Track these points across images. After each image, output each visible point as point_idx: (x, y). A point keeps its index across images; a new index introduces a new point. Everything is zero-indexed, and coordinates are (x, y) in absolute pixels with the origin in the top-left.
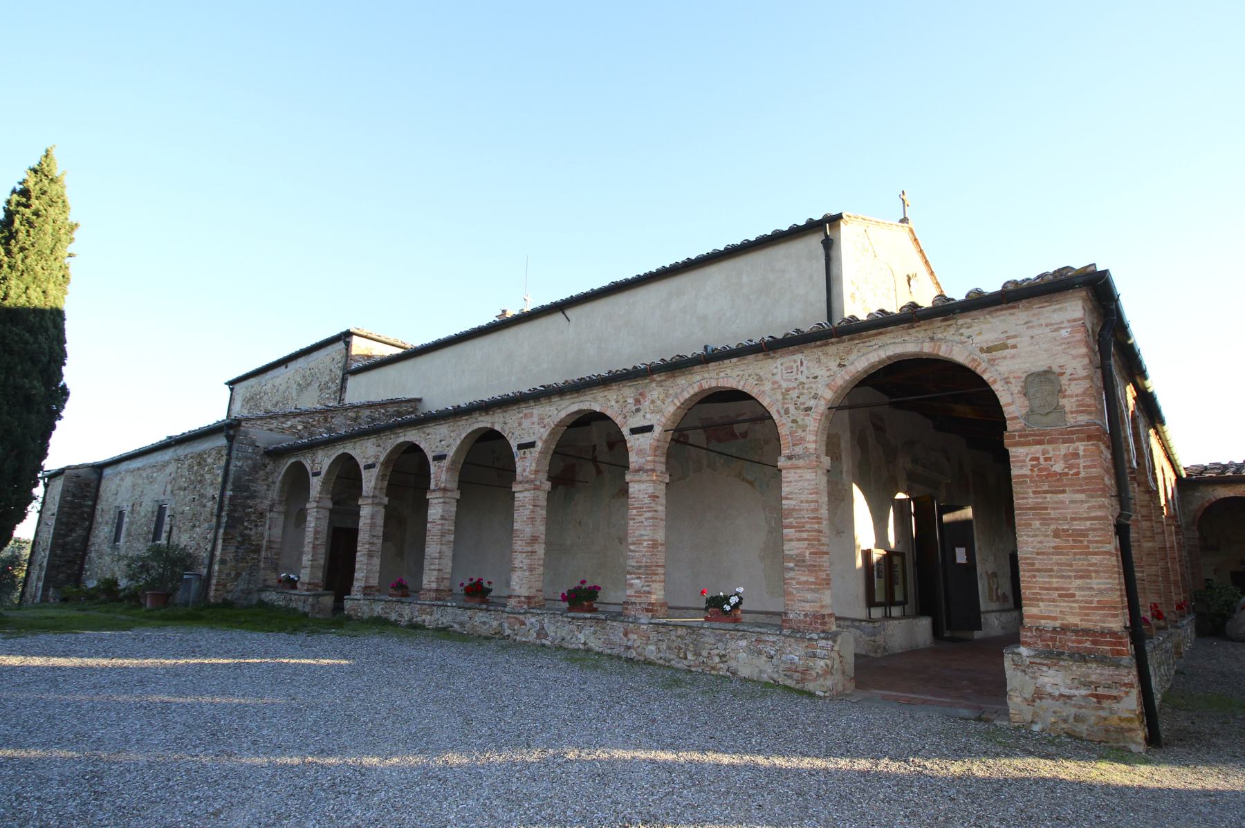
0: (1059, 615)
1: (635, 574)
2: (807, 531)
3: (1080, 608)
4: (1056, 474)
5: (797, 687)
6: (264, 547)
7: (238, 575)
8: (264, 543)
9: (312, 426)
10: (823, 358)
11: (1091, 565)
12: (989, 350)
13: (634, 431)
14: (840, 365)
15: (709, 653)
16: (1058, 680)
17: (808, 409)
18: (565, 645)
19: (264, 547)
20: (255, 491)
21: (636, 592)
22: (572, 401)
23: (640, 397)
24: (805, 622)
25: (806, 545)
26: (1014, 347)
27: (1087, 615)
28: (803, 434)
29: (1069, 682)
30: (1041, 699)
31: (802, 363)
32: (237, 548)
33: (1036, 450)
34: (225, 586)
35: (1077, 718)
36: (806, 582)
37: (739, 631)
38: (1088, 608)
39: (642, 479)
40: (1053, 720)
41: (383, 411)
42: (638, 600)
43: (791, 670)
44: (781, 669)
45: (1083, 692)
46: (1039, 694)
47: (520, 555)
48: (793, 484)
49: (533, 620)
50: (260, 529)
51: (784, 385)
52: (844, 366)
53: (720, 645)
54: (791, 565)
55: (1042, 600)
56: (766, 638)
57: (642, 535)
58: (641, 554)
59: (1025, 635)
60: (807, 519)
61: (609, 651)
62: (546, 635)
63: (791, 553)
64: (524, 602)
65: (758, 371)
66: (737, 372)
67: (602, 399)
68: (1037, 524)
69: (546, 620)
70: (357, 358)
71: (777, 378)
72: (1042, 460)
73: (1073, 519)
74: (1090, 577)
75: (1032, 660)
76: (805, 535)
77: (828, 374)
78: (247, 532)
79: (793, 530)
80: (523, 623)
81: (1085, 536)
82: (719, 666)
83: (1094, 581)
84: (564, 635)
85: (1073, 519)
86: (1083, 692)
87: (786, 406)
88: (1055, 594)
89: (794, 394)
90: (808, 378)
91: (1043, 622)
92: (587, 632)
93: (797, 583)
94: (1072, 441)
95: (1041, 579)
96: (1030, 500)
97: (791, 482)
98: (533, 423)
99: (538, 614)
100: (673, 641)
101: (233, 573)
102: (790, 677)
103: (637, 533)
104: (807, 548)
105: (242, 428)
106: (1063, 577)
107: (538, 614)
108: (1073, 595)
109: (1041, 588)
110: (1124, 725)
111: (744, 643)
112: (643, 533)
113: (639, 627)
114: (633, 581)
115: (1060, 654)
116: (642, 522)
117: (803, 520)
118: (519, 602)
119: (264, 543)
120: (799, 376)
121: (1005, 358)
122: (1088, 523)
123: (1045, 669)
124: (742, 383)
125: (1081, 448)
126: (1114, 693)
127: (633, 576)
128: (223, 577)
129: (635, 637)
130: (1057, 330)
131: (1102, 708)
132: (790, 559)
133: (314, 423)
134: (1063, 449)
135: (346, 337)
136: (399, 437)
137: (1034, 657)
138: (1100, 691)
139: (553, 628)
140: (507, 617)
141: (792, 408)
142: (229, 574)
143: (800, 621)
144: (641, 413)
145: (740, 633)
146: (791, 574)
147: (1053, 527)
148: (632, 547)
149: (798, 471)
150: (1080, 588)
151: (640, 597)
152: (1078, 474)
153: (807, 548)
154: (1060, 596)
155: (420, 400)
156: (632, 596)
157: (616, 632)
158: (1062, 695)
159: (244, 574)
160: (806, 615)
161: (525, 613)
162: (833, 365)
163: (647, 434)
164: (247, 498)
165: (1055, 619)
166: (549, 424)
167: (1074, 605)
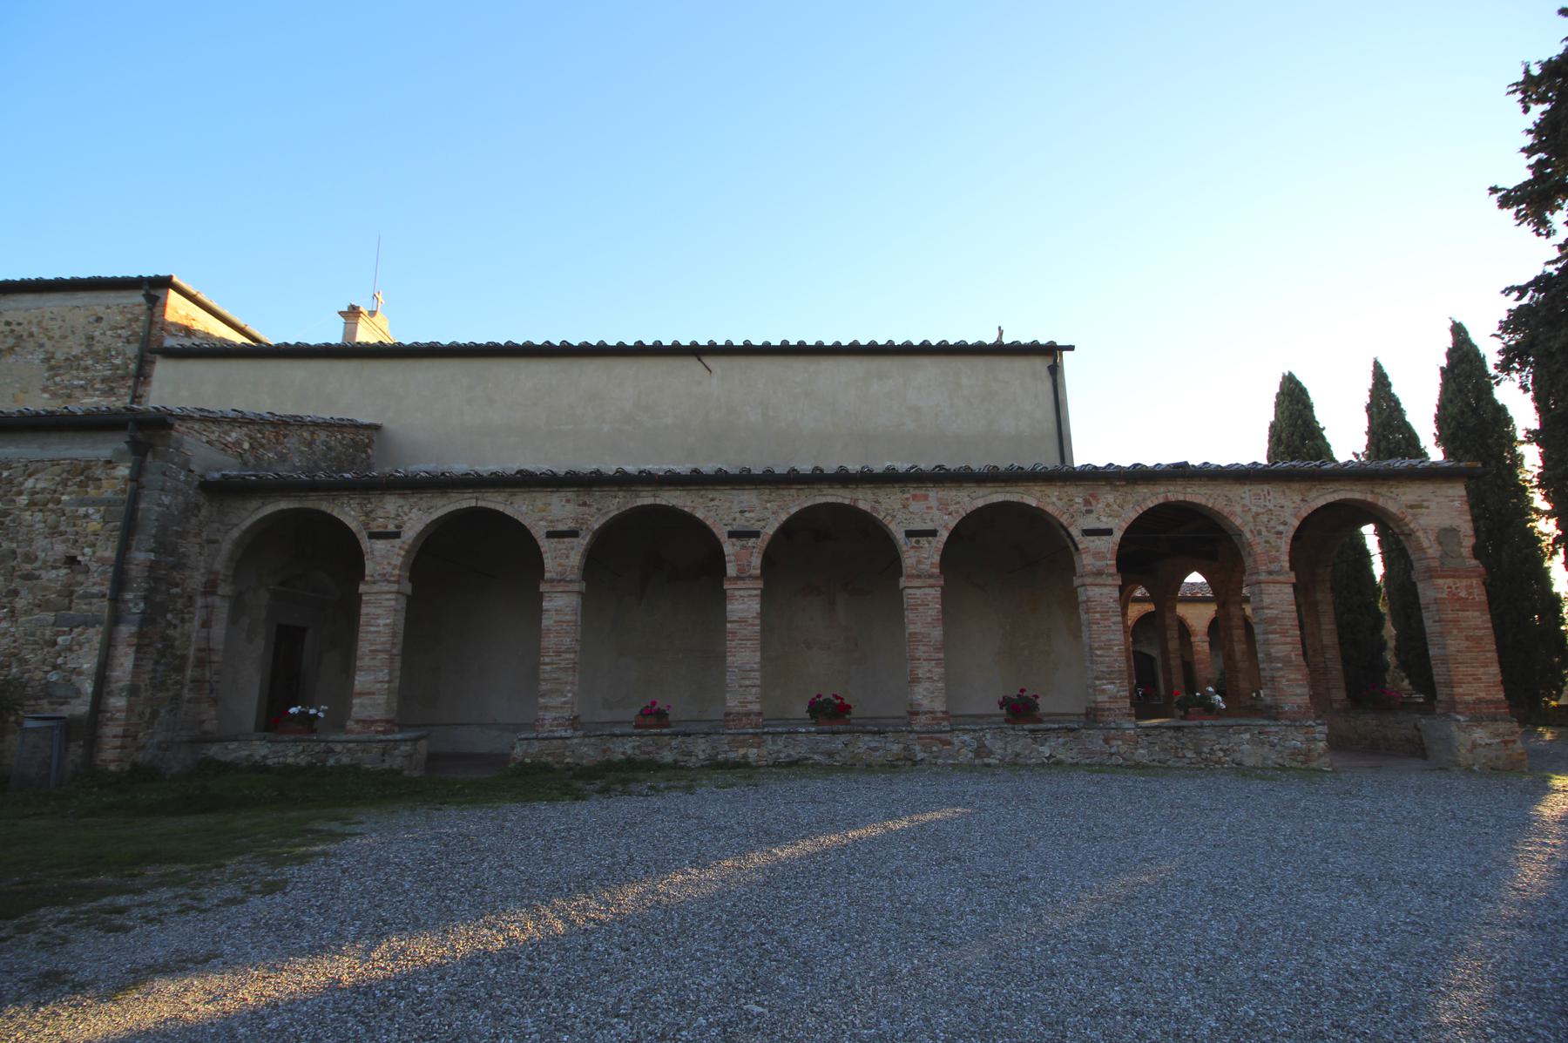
0: (1473, 692)
1: (1106, 679)
2: (1291, 636)
3: (1485, 686)
4: (1462, 598)
5: (1303, 767)
6: (191, 660)
7: (155, 714)
8: (191, 652)
9: (262, 446)
10: (1287, 491)
11: (1487, 658)
12: (1411, 507)
13: (1088, 533)
14: (1303, 500)
15: (1212, 749)
16: (1482, 735)
17: (1280, 533)
18: (1021, 761)
19: (191, 660)
20: (184, 555)
21: (1110, 697)
22: (994, 489)
23: (1091, 499)
24: (1299, 713)
25: (1291, 649)
26: (1427, 508)
27: (1489, 691)
28: (1277, 554)
29: (1488, 734)
30: (1475, 748)
31: (1269, 493)
32: (157, 662)
33: (1450, 581)
34: (135, 738)
35: (1497, 758)
36: (1296, 679)
37: (1241, 725)
38: (1489, 686)
39: (1107, 583)
40: (1484, 761)
41: (339, 437)
42: (1113, 706)
43: (1295, 753)
44: (1285, 754)
45: (1498, 740)
46: (1475, 746)
47: (925, 663)
48: (1273, 596)
49: (966, 737)
50: (187, 626)
51: (1254, 509)
52: (1306, 501)
53: (1222, 740)
54: (1280, 665)
55: (1464, 683)
56: (1268, 729)
57: (1110, 640)
58: (1112, 659)
59: (1460, 707)
60: (1289, 627)
61: (1088, 761)
62: (990, 754)
63: (1279, 655)
64: (943, 719)
65: (1227, 493)
66: (1204, 490)
67: (1039, 494)
68: (1455, 632)
69: (988, 736)
70: (173, 329)
71: (1247, 502)
72: (1454, 589)
73: (1475, 629)
74: (1487, 666)
75: (1470, 723)
76: (1289, 640)
77: (1293, 505)
78: (170, 632)
79: (1277, 636)
80: (950, 743)
81: (1482, 639)
82: (1223, 759)
83: (1491, 669)
84: (1018, 750)
85: (1475, 629)
86: (1498, 740)
87: (1258, 528)
88: (1470, 678)
89: (1265, 518)
90: (1275, 506)
91: (1466, 697)
92: (1053, 744)
93: (1287, 681)
94: (1471, 577)
95: (1462, 669)
96: (1450, 616)
97: (1271, 594)
98: (929, 508)
99: (975, 731)
100: (1167, 743)
101: (148, 711)
102: (1295, 760)
103: (1104, 638)
104: (1292, 651)
105: (174, 433)
106: (1473, 667)
107: (975, 731)
108: (1480, 679)
109: (1463, 675)
110: (1520, 757)
111: (1247, 736)
112: (1112, 637)
113: (1124, 732)
114: (1104, 687)
115: (1482, 719)
116: (1110, 627)
117: (1286, 627)
118: (934, 719)
119: (191, 652)
120: (1267, 504)
121: (1422, 514)
122: (1483, 631)
123: (1475, 728)
124: (1212, 501)
125: (1475, 582)
126: (1512, 738)
127: (1105, 682)
128: (134, 720)
129: (1120, 743)
130: (1452, 501)
131: (1508, 749)
132: (1278, 659)
133: (264, 441)
134: (1465, 582)
135: (156, 287)
136: (638, 497)
137: (1469, 721)
138: (1506, 738)
139: (1000, 744)
140: (919, 738)
141: (1264, 530)
142: (141, 715)
143: (1295, 713)
144: (1094, 516)
145: (1243, 728)
146: (1281, 673)
147: (1464, 634)
148: (1098, 652)
149: (1278, 585)
150: (1484, 674)
151: (1116, 702)
152: (1474, 599)
153: (1292, 651)
154: (1475, 679)
155: (377, 428)
156: (1106, 702)
157: (1095, 740)
158: (1487, 744)
159: (163, 712)
160: (1299, 707)
161: (952, 731)
162: (1297, 498)
163: (1105, 538)
164: (174, 567)
165: (1472, 695)
166: (957, 512)
167: (1482, 685)
